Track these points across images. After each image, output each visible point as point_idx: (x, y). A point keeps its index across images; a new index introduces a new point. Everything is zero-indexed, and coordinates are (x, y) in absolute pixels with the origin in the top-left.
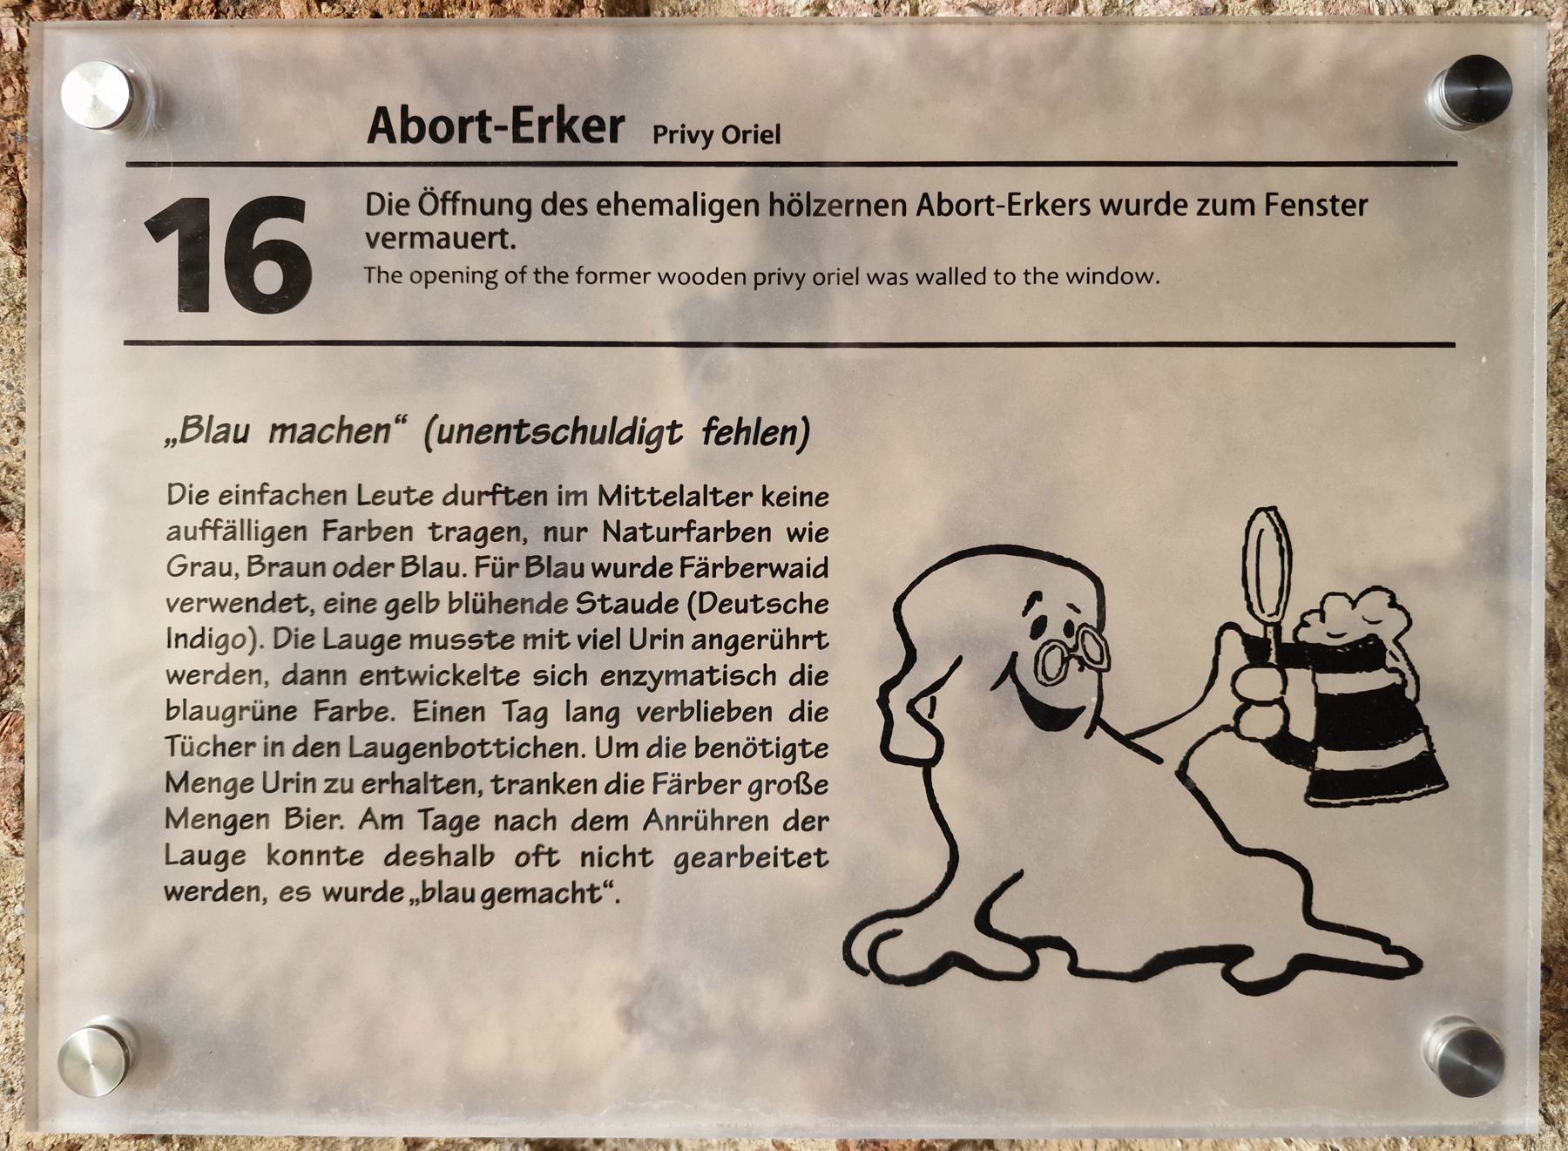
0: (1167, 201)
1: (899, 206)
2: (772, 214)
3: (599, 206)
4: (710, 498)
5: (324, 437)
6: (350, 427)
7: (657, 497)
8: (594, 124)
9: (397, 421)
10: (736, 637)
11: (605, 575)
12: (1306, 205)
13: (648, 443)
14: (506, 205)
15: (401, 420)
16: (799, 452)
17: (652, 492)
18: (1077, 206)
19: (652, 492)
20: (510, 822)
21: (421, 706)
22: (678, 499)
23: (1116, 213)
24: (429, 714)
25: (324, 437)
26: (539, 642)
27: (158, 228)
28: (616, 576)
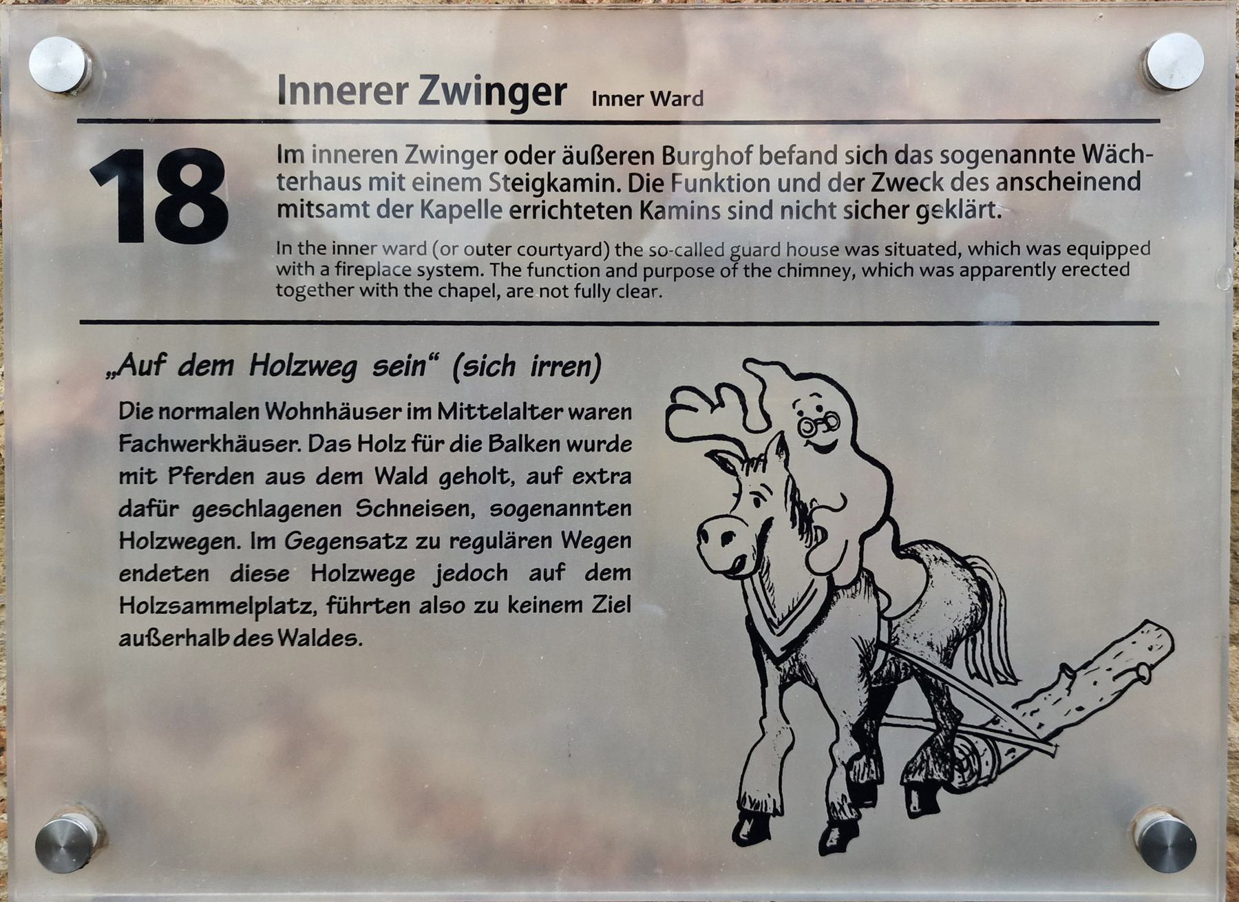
2: (783, 217)
3: (414, 184)
4: (529, 413)
7: (486, 412)
8: (384, 89)
9: (431, 358)
10: (526, 506)
11: (578, 449)
12: (1017, 182)
13: (345, 374)
15: (434, 357)
16: (592, 382)
17: (482, 408)
19: (482, 408)
22: (502, 413)
25: (492, 371)
26: (132, 478)
27: (101, 175)
28: (587, 450)
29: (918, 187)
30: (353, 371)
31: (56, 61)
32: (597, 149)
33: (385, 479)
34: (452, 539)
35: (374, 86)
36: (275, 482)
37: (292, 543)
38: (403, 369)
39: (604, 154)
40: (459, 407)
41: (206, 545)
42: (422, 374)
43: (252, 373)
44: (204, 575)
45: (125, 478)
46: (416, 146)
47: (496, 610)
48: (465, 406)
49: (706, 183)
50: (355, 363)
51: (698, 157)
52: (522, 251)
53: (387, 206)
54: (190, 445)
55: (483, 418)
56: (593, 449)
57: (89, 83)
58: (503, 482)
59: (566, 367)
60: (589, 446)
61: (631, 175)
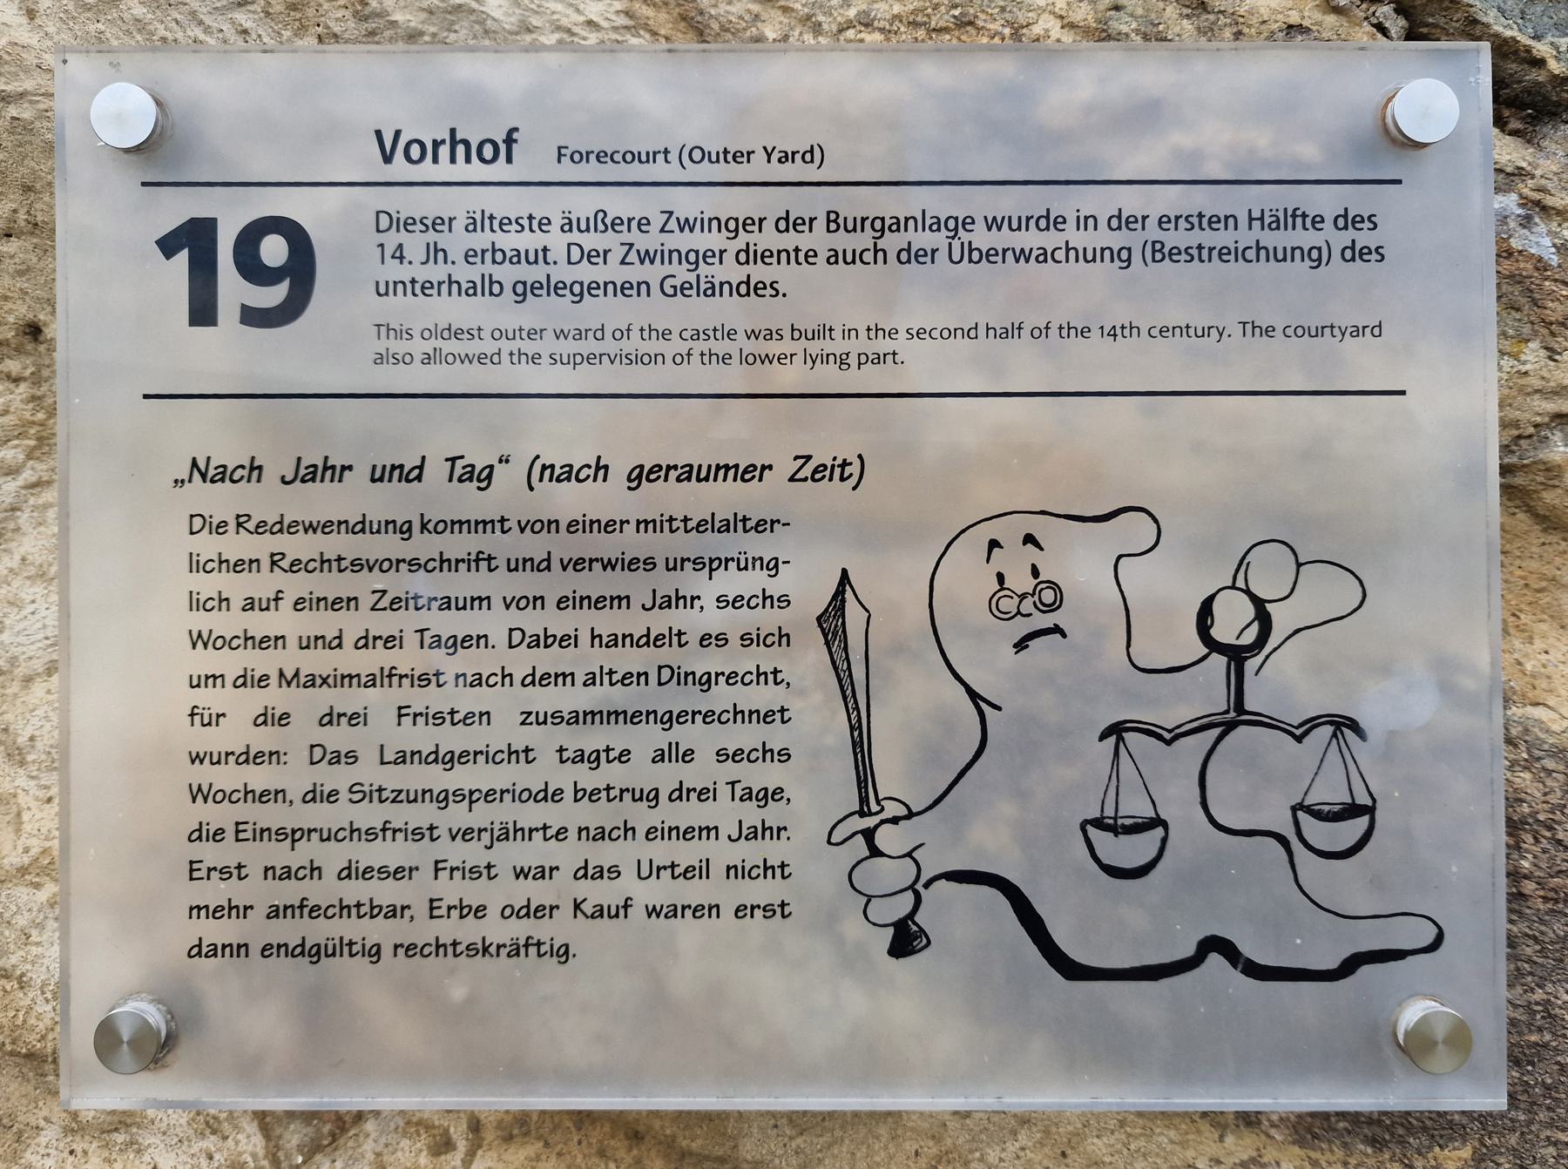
1: (644, 287)
5: (236, 477)
7: (690, 525)
9: (500, 461)
13: (479, 480)
14: (1107, 253)
15: (504, 460)
17: (686, 520)
18: (1182, 221)
19: (686, 520)
20: (278, 872)
24: (249, 835)
25: (236, 477)
27: (168, 246)
31: (120, 110)
32: (601, 215)
36: (449, 608)
39: (608, 221)
44: (485, 718)
46: (671, 213)
49: (911, 222)
51: (868, 224)
52: (1153, 332)
53: (1353, 248)
54: (324, 526)
55: (686, 531)
57: (161, 134)
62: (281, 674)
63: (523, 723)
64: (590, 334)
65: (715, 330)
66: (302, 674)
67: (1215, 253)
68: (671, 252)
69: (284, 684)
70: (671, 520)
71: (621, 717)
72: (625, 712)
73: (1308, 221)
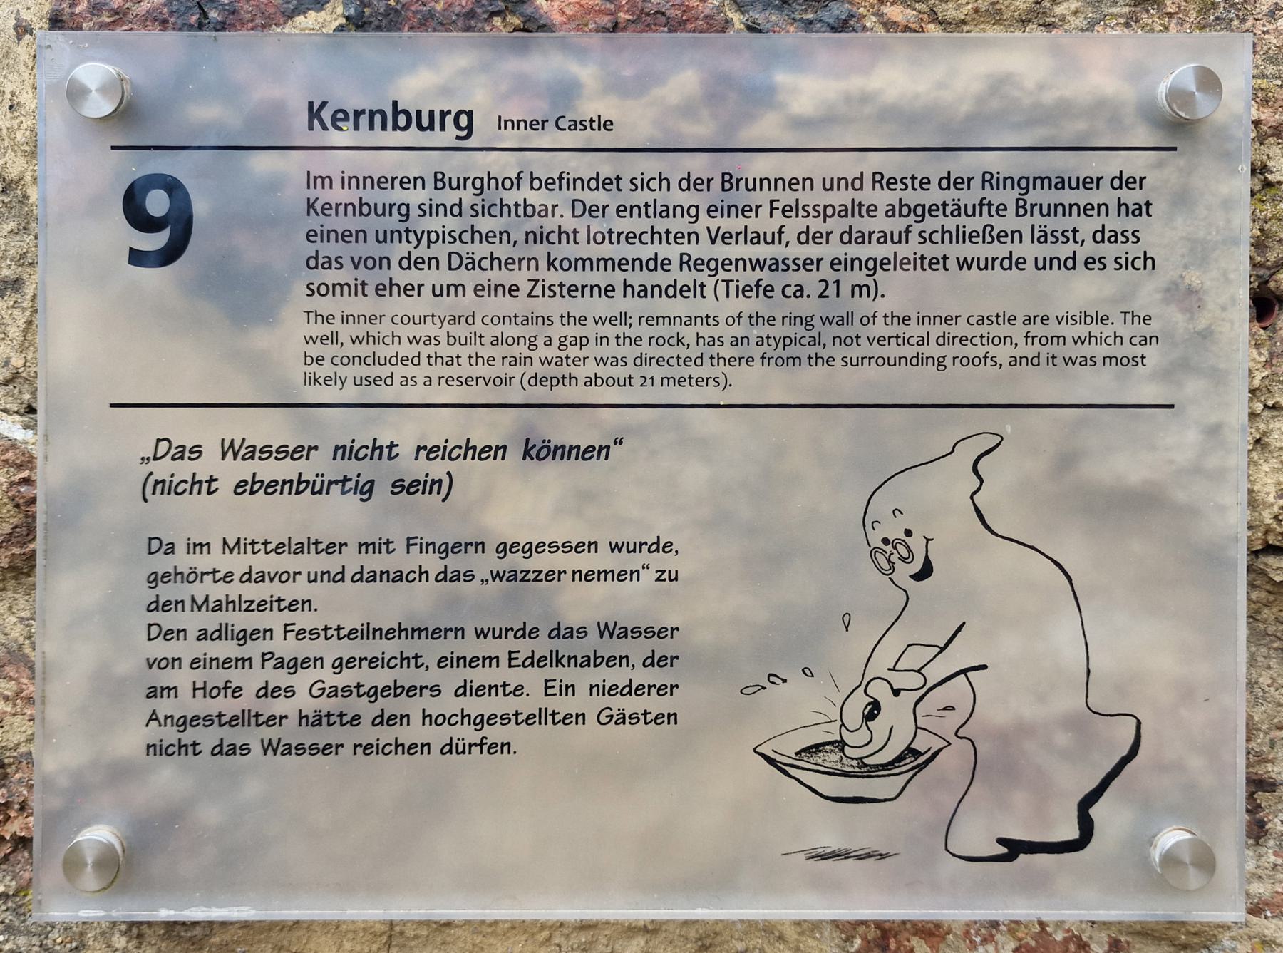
0: (1010, 259)
4: (313, 547)
6: (474, 448)
16: (444, 500)
21: (550, 684)
22: (286, 548)
23: (969, 268)
24: (556, 690)
26: (371, 548)
29: (637, 240)
30: (370, 490)
32: (988, 229)
33: (270, 751)
34: (356, 746)
35: (453, 113)
37: (603, 719)
38: (421, 487)
39: (995, 234)
40: (242, 542)
41: (295, 665)
42: (503, 458)
43: (416, 459)
45: (363, 548)
47: (676, 579)
48: (249, 541)
50: (372, 482)
55: (267, 553)
56: (500, 637)
58: (417, 667)
59: (430, 452)
60: (631, 548)
61: (450, 254)
62: (193, 600)
63: (658, 580)
64: (463, 319)
65: (998, 316)
66: (211, 600)
67: (623, 237)
68: (438, 206)
69: (195, 608)
70: (253, 543)
71: (610, 575)
72: (612, 571)
73: (993, 209)
